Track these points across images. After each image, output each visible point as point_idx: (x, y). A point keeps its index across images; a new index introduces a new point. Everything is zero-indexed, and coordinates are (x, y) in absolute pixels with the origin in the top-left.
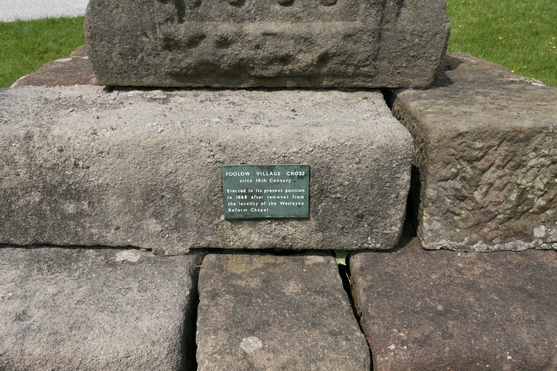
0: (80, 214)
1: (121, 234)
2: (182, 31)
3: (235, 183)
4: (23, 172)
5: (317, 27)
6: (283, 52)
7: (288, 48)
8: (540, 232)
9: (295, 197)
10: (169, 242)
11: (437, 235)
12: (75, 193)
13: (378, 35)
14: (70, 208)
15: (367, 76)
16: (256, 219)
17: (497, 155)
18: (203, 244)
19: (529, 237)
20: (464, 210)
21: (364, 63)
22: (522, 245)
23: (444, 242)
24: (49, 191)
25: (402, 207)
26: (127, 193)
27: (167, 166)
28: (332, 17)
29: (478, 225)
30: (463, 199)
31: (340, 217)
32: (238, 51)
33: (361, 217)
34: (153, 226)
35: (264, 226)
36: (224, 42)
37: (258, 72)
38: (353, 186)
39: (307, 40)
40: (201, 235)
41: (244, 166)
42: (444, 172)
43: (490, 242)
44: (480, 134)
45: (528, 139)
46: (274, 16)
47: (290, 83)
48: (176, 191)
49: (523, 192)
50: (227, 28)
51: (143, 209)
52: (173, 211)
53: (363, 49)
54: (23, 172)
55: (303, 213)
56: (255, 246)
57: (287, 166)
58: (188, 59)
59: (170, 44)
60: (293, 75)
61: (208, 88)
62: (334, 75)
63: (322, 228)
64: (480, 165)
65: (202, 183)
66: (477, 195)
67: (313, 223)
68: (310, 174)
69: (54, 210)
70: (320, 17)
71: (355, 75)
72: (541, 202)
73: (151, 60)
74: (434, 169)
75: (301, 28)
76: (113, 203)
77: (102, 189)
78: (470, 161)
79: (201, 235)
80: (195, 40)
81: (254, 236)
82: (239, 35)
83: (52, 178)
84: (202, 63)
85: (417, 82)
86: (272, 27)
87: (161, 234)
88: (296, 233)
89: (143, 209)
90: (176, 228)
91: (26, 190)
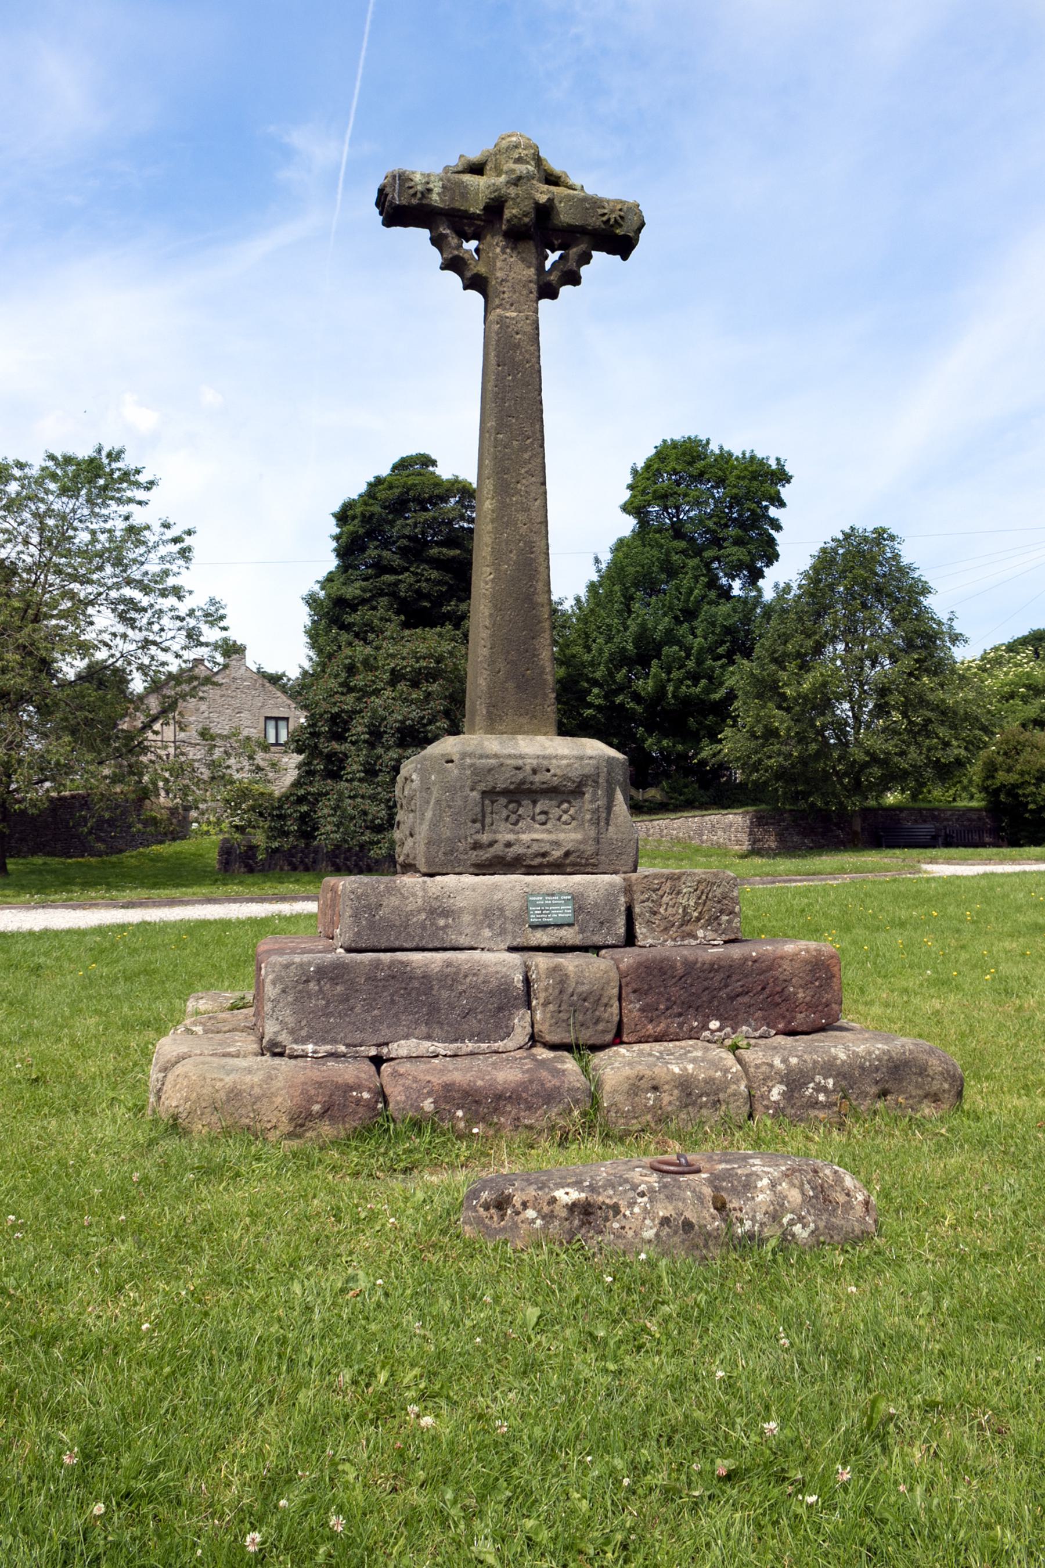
0: (446, 926)
1: (468, 939)
2: (485, 838)
4: (419, 901)
5: (562, 836)
6: (543, 850)
7: (547, 848)
8: (700, 933)
9: (565, 912)
10: (496, 943)
12: (446, 913)
13: (597, 841)
14: (442, 922)
15: (594, 865)
16: (545, 926)
17: (667, 887)
18: (515, 944)
19: (695, 937)
20: (656, 920)
21: (591, 857)
22: (694, 942)
23: (650, 941)
24: (432, 912)
25: (624, 917)
26: (475, 913)
27: (498, 896)
28: (570, 831)
29: (666, 929)
30: (655, 913)
31: (591, 924)
32: (517, 850)
33: (602, 923)
34: (487, 933)
35: (549, 930)
36: (509, 845)
37: (528, 862)
38: (596, 904)
39: (557, 844)
40: (514, 938)
41: (538, 895)
42: (642, 898)
43: (674, 940)
44: (656, 876)
45: (679, 878)
46: (536, 831)
47: (547, 871)
48: (502, 910)
49: (685, 908)
50: (511, 837)
51: (482, 922)
52: (499, 923)
53: (589, 849)
54: (419, 901)
55: (571, 921)
56: (545, 944)
57: (561, 893)
58: (486, 855)
59: (477, 846)
60: (550, 865)
62: (574, 864)
63: (582, 931)
64: (660, 893)
65: (517, 904)
66: (662, 910)
67: (576, 928)
68: (573, 898)
69: (432, 924)
70: (563, 831)
71: (586, 865)
72: (696, 914)
73: (462, 857)
75: (553, 837)
76: (466, 918)
77: (461, 910)
78: (654, 891)
79: (514, 938)
80: (491, 844)
81: (543, 938)
82: (518, 841)
83: (435, 904)
84: (497, 857)
85: (624, 869)
86: (536, 836)
87: (491, 938)
88: (568, 935)
89: (482, 922)
90: (500, 934)
91: (419, 912)
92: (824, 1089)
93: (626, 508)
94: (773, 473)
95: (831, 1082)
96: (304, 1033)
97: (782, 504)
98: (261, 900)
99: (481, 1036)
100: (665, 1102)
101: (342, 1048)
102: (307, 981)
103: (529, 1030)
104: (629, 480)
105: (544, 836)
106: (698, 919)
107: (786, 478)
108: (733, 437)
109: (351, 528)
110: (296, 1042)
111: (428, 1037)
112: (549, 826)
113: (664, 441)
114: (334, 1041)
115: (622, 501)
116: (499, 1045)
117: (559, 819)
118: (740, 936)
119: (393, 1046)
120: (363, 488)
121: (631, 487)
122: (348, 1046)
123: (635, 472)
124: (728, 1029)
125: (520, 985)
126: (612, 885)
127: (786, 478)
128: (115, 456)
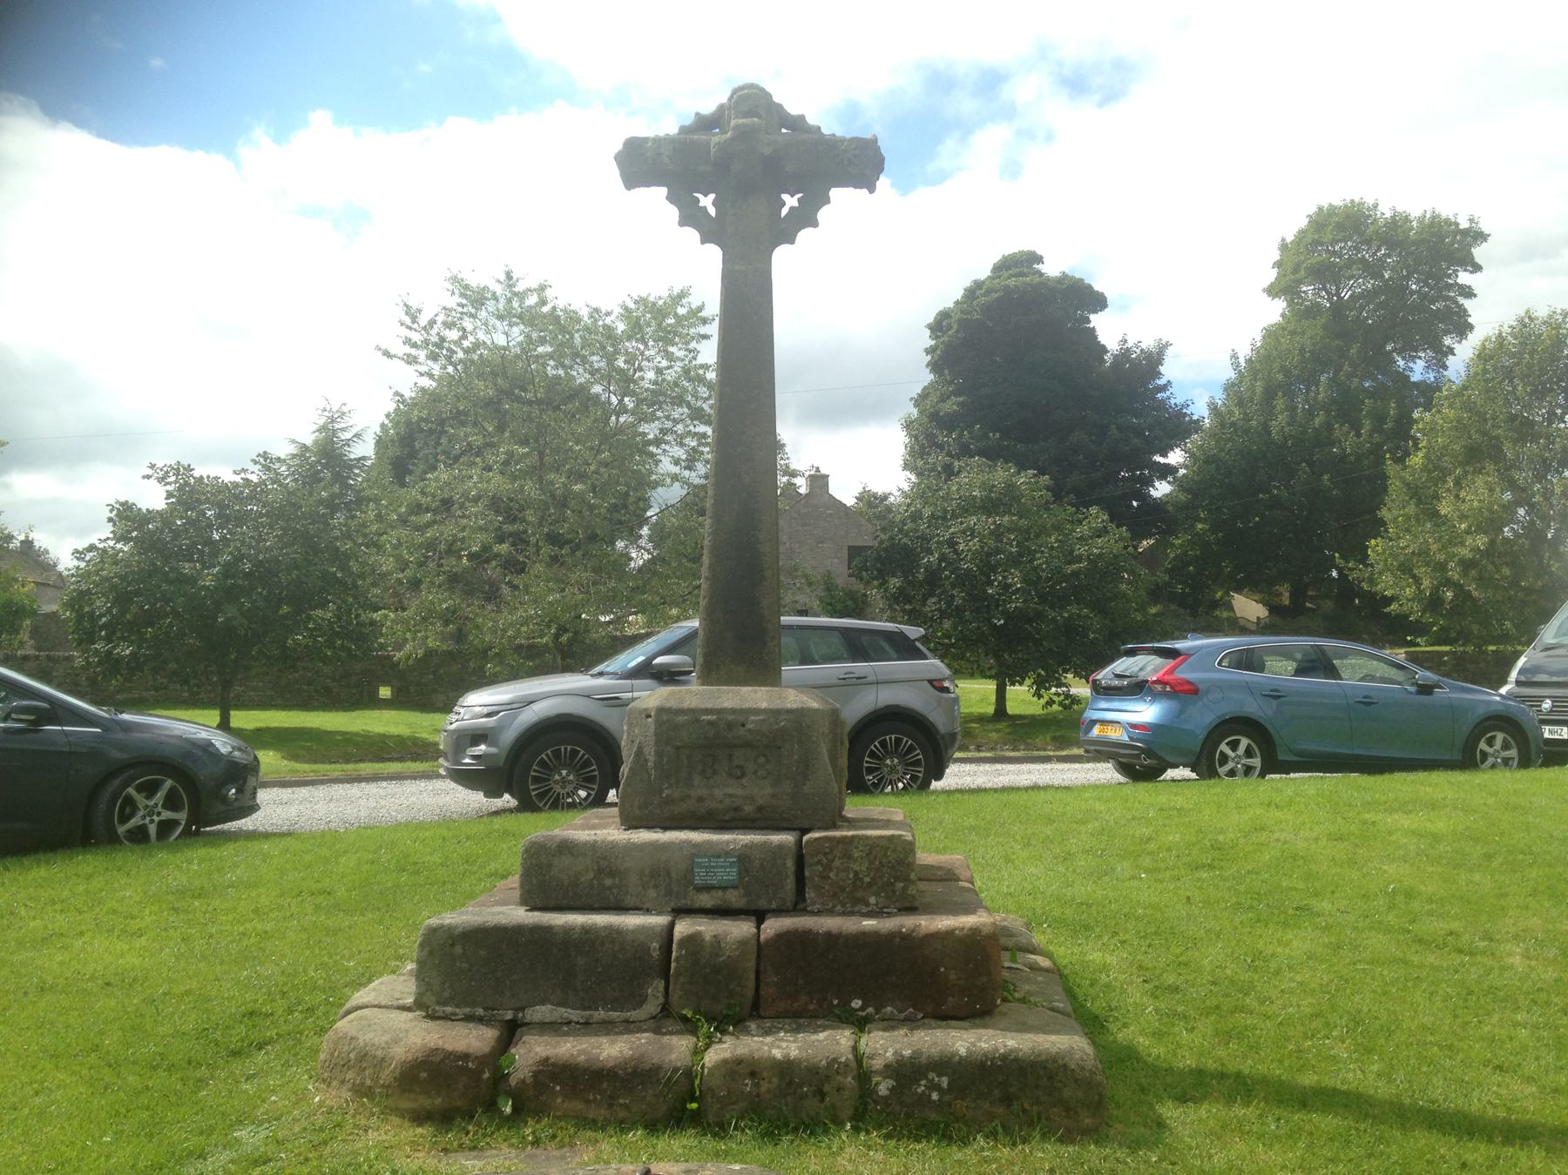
3: (700, 865)
8: (872, 900)
9: (731, 875)
11: (813, 903)
12: (612, 874)
16: (709, 888)
29: (835, 895)
34: (652, 893)
35: (714, 893)
36: (700, 799)
41: (705, 856)
48: (668, 874)
49: (856, 873)
50: (702, 792)
56: (709, 905)
61: (421, 826)
72: (867, 880)
74: (808, 860)
78: (825, 854)
81: (705, 900)
86: (730, 791)
88: (735, 898)
92: (938, 1087)
93: (1273, 291)
94: (1465, 232)
95: (945, 1081)
96: (446, 994)
97: (1477, 268)
98: (1296, 633)
99: (618, 1004)
100: (763, 1090)
101: (480, 1011)
102: (452, 945)
103: (661, 999)
104: (1276, 256)
105: (739, 791)
106: (869, 884)
107: (1481, 237)
108: (1405, 194)
109: (945, 339)
110: (439, 1003)
111: (564, 1004)
112: (744, 781)
113: (1320, 209)
114: (473, 1004)
115: (1266, 284)
116: (633, 1015)
117: (755, 772)
118: (917, 904)
119: (529, 1012)
120: (958, 294)
121: (1278, 264)
122: (486, 1009)
123: (1284, 247)
124: (870, 1010)
125: (655, 954)
126: (781, 847)
127: (1481, 237)
128: (683, 295)
